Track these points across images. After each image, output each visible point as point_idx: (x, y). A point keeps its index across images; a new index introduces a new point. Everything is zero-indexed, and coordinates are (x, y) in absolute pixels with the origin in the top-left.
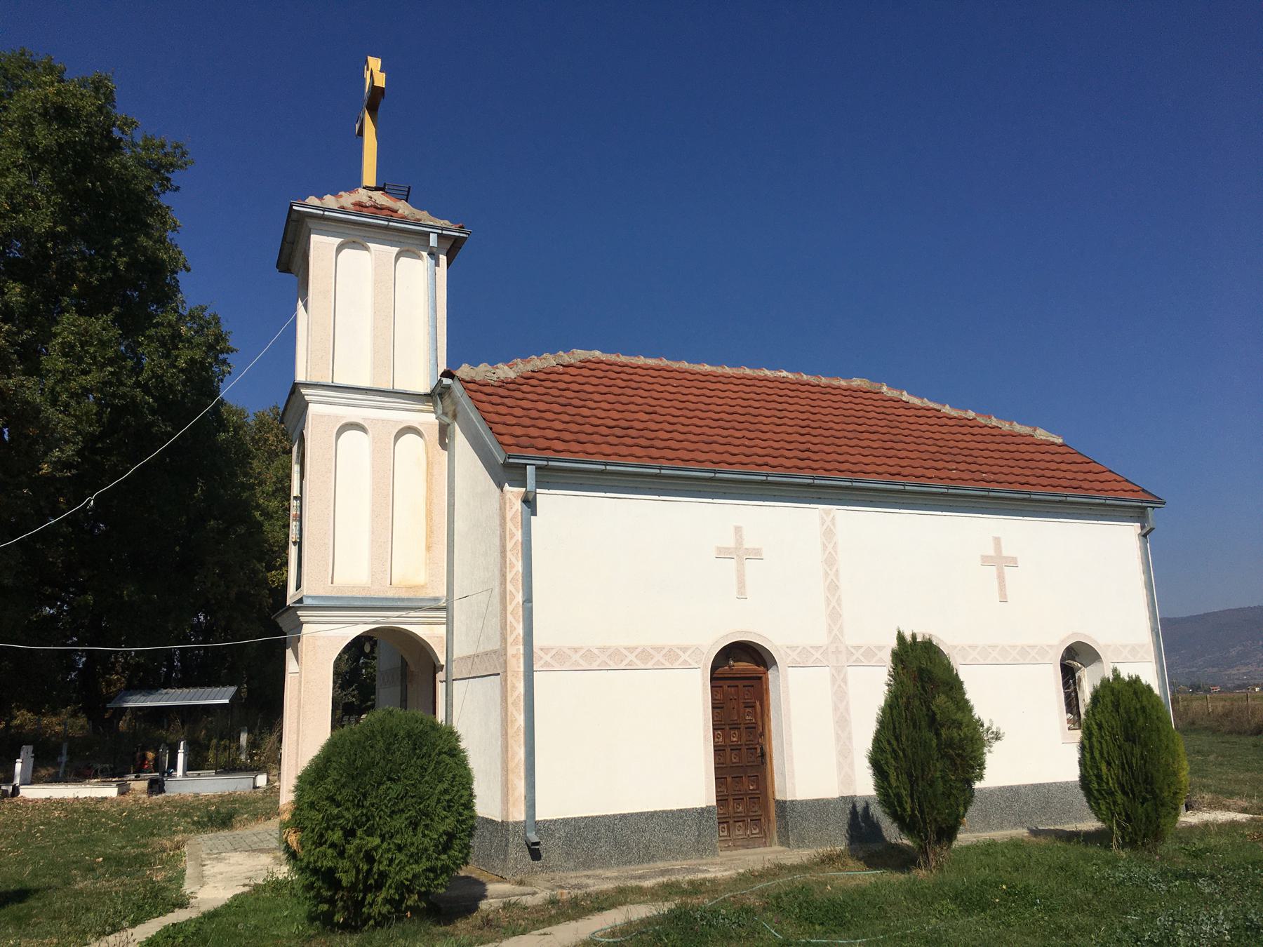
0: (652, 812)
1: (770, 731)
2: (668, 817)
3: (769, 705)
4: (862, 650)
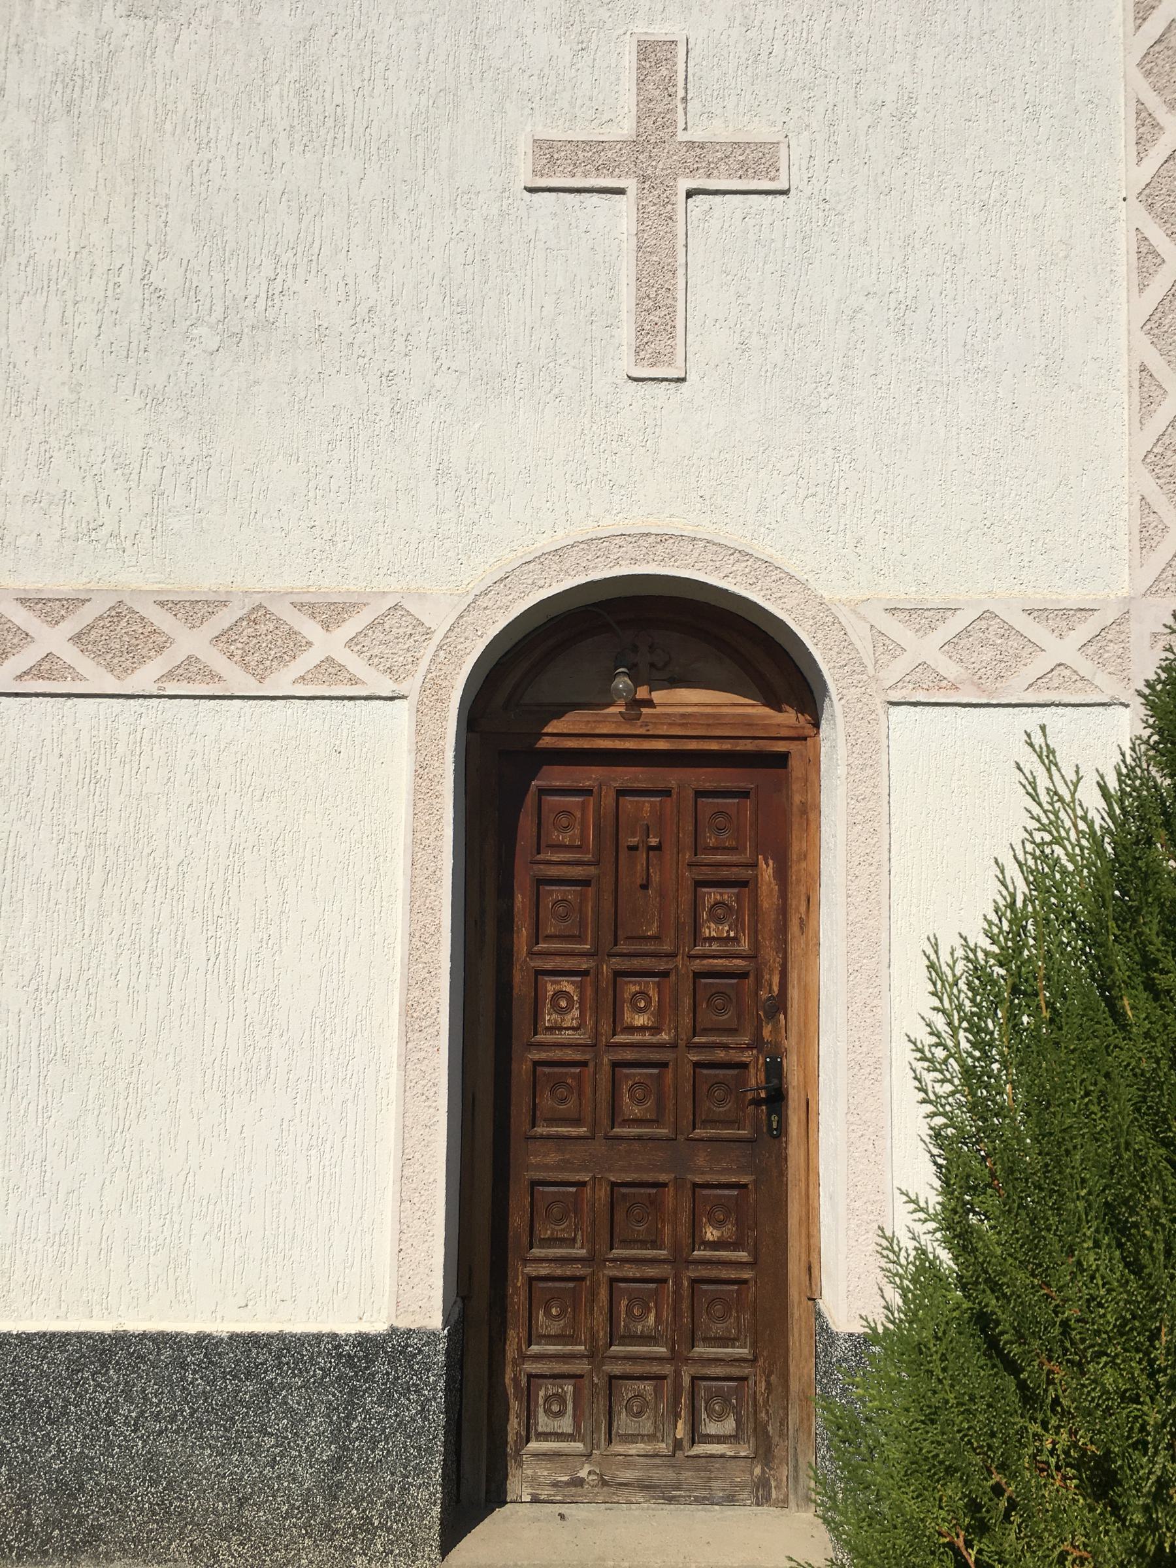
0: (102, 1337)
1: (811, 994)
2: (184, 1366)
3: (813, 879)
4: (1085, 630)
